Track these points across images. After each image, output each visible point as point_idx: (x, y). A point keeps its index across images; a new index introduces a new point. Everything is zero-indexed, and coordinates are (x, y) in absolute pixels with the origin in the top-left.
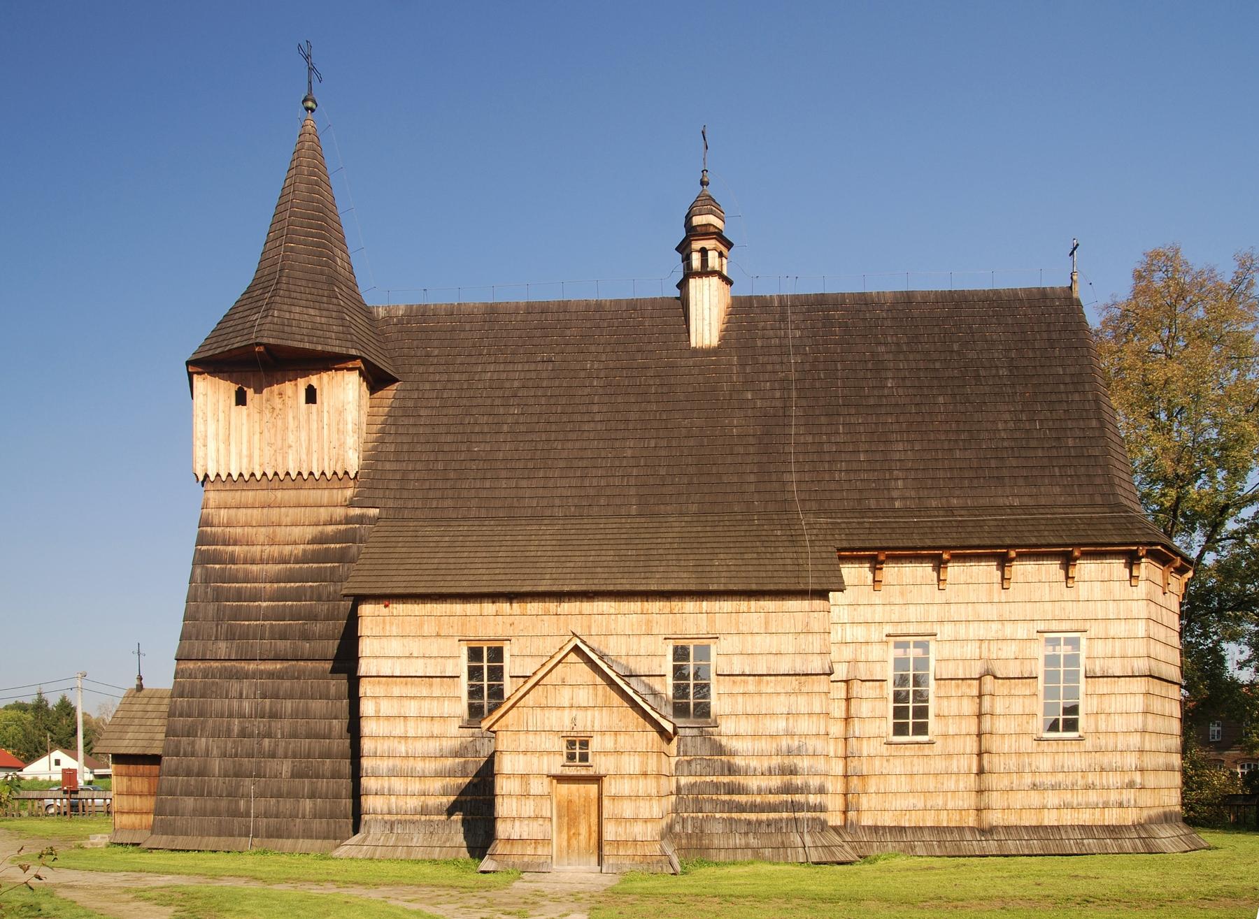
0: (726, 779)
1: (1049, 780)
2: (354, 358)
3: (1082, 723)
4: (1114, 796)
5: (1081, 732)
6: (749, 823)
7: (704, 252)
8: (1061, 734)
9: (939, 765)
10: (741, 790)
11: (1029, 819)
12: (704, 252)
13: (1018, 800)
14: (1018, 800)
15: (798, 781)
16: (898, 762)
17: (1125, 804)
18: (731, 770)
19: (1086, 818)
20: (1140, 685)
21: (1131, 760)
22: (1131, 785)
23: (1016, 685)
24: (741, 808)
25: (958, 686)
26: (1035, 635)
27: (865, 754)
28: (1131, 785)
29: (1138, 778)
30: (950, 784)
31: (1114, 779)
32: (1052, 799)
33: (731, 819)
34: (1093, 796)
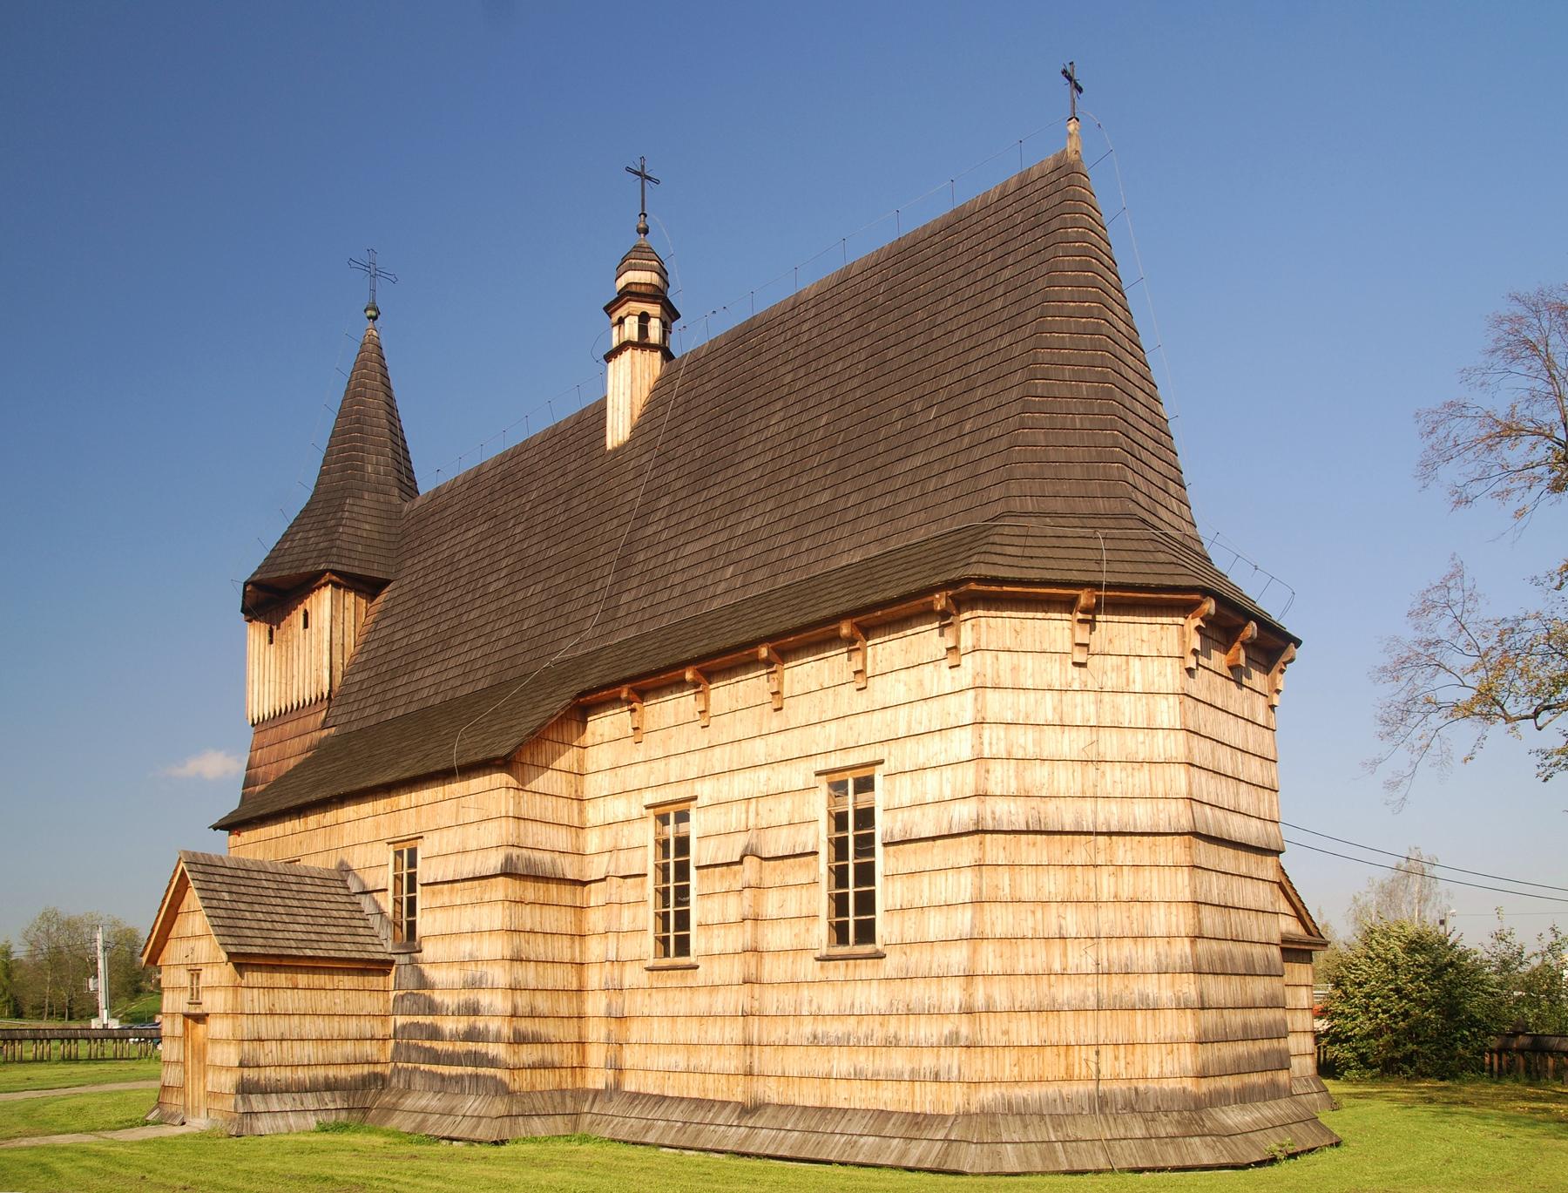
0: (428, 1020)
1: (835, 1029)
2: (324, 572)
3: (880, 929)
4: (927, 1061)
5: (879, 945)
6: (442, 1077)
7: (644, 318)
8: (851, 948)
9: (702, 1002)
10: (435, 1034)
11: (809, 1096)
12: (644, 318)
13: (794, 1062)
14: (794, 1062)
15: (480, 1023)
16: (658, 997)
17: (944, 1076)
18: (432, 1009)
19: (888, 1097)
20: (1174, 850)
21: (953, 994)
22: (952, 1042)
23: (452, 891)
24: (437, 1058)
25: (452, 891)
26: (813, 781)
27: (626, 986)
28: (952, 1042)
29: (965, 1028)
30: (714, 1033)
31: (928, 1030)
32: (841, 1062)
33: (477, 1076)
34: (899, 1061)
